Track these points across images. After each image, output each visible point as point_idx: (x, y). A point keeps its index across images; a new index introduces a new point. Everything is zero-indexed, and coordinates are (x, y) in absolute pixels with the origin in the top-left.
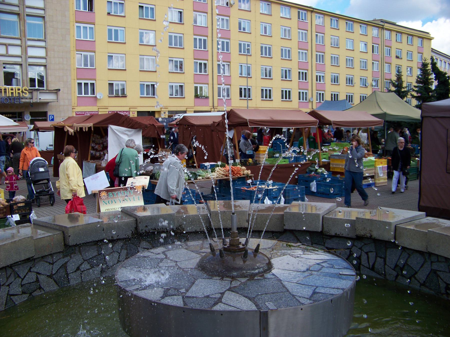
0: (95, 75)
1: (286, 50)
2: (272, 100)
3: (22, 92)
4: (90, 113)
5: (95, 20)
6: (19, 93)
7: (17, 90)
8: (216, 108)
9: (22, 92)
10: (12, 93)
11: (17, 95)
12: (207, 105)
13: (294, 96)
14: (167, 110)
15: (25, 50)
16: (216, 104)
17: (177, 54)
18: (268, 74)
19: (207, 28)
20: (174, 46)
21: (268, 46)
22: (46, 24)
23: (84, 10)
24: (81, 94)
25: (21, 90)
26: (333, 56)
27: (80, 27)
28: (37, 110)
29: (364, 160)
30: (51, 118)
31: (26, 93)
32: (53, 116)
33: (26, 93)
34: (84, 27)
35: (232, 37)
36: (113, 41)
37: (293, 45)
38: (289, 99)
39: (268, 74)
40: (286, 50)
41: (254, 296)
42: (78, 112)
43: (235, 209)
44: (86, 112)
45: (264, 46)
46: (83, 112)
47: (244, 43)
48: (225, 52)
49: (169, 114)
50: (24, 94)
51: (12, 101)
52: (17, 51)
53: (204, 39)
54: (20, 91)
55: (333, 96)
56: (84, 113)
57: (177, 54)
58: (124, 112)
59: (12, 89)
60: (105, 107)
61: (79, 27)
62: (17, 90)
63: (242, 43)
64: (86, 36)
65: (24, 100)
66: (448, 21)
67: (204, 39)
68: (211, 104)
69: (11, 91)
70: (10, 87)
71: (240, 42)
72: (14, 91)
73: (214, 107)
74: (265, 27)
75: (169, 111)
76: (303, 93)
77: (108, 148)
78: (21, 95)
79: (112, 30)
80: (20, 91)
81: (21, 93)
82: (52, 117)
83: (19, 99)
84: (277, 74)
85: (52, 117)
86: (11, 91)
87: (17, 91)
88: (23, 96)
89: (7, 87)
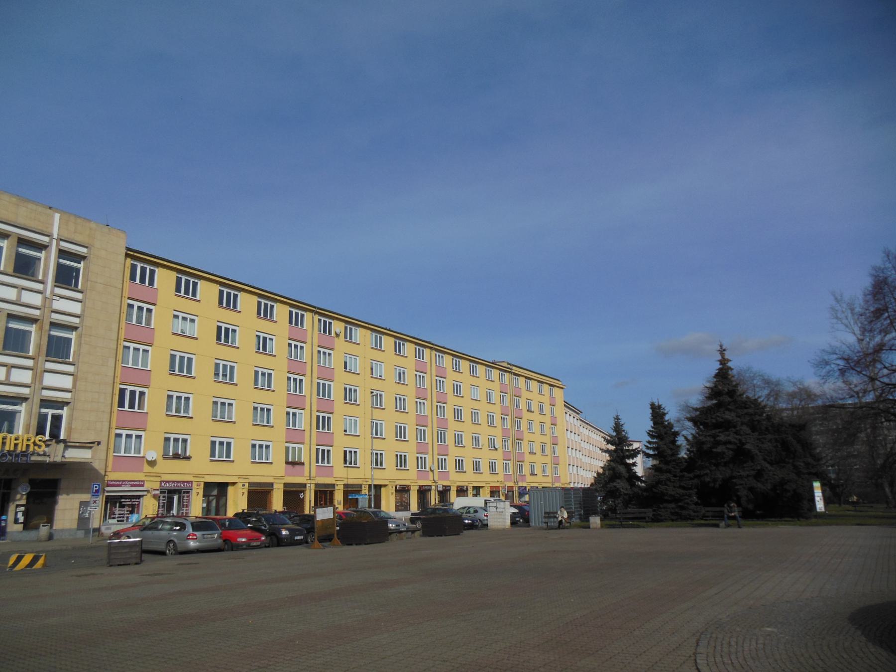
0: (332, 440)
4: (130, 483)
8: (314, 479)
10: (16, 445)
11: (24, 449)
12: (302, 475)
13: (411, 463)
14: (247, 481)
16: (313, 474)
17: (262, 397)
18: (376, 432)
21: (229, 364)
24: (378, 466)
26: (456, 408)
27: (129, 348)
30: (95, 489)
31: (40, 446)
32: (99, 485)
33: (40, 446)
35: (336, 378)
36: (185, 374)
37: (409, 392)
38: (380, 466)
39: (376, 432)
42: (112, 481)
44: (124, 481)
46: (119, 481)
47: (351, 387)
48: (326, 398)
50: (36, 448)
53: (268, 373)
54: (30, 443)
55: (440, 467)
56: (121, 483)
57: (262, 397)
58: (184, 482)
60: (155, 474)
63: (222, 363)
64: (135, 362)
65: (34, 458)
67: (268, 373)
68: (307, 474)
71: (257, 369)
73: (312, 478)
74: (399, 373)
80: (30, 443)
81: (32, 445)
83: (26, 456)
85: (96, 487)
87: (25, 442)
88: (34, 449)
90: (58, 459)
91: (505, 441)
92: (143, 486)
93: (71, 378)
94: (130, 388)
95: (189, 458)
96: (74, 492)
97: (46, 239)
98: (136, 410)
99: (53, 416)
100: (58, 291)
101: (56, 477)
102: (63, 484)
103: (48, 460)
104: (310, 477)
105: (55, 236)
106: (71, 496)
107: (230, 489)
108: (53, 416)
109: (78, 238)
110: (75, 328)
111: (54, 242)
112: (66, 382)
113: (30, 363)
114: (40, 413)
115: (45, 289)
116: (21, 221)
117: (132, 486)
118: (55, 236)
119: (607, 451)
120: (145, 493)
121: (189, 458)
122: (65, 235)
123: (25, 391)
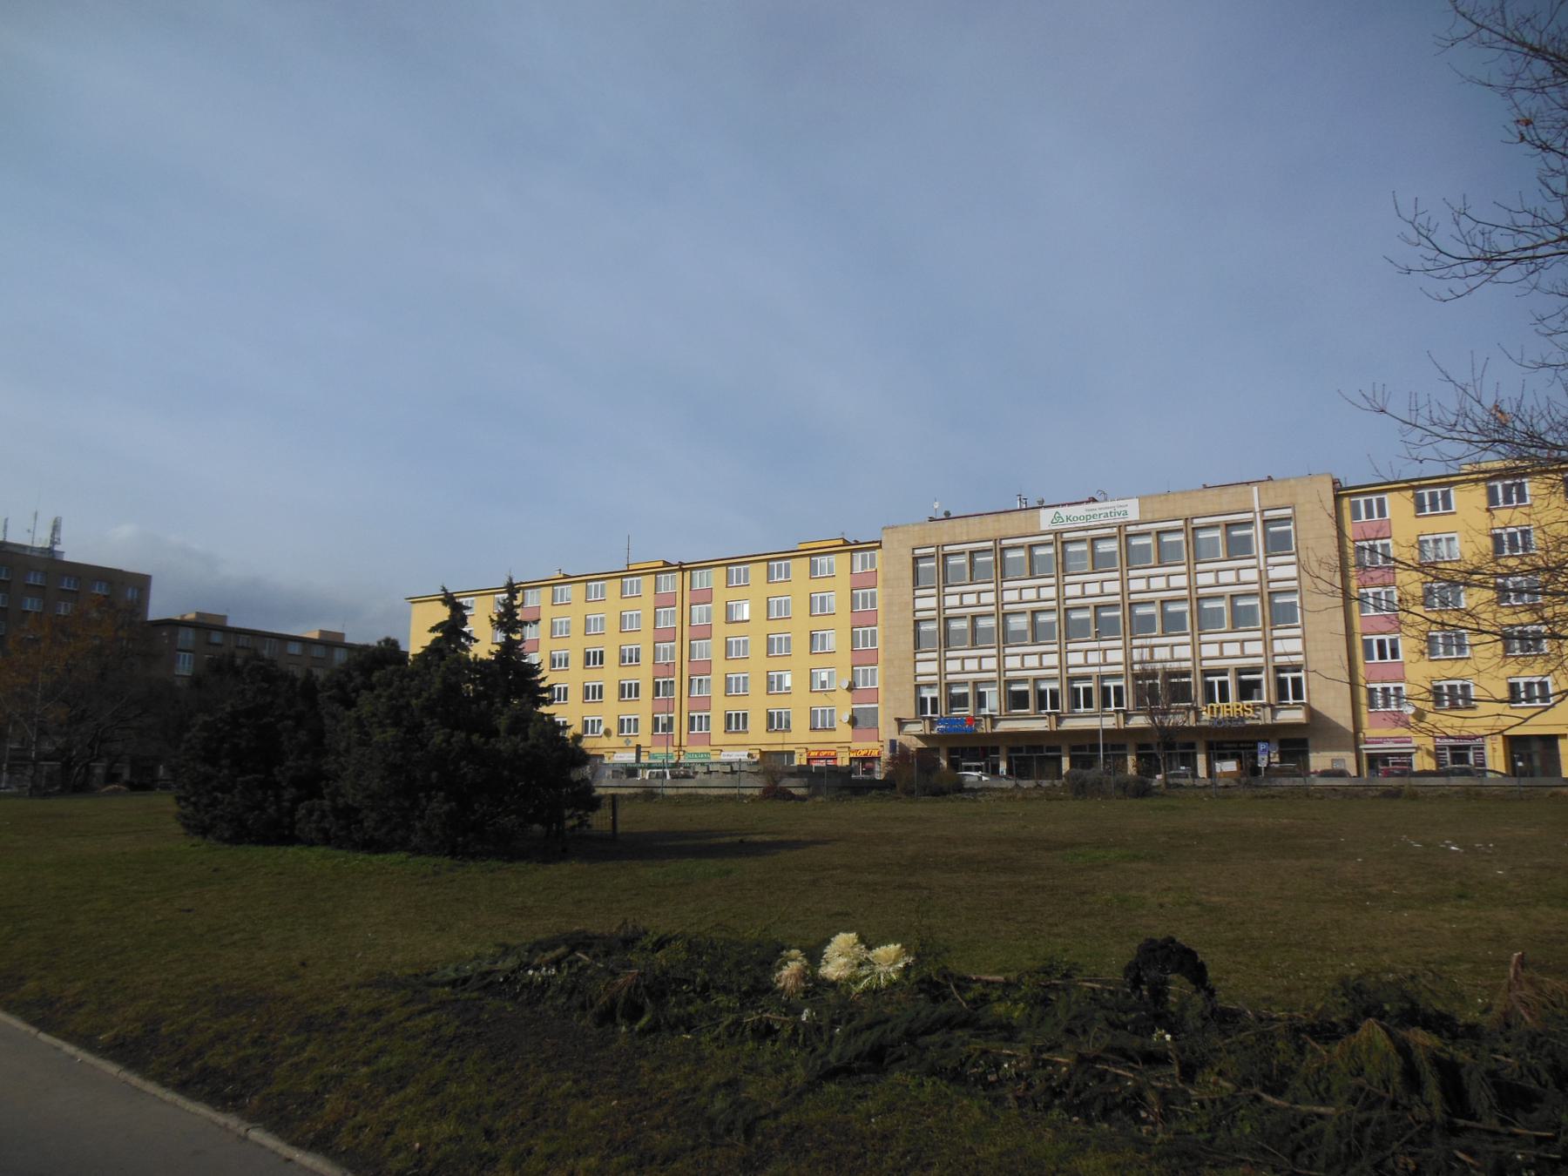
2: (1454, 513)
3: (1244, 710)
9: (1244, 710)
23: (1180, 556)
28: (1290, 736)
29: (453, 740)
31: (1249, 712)
33: (1249, 712)
41: (676, 759)
43: (1230, 1081)
51: (1228, 723)
54: (1240, 709)
59: (1228, 707)
65: (1248, 722)
66: (26, 533)
69: (1236, 709)
70: (1225, 704)
72: (1231, 710)
76: (700, 717)
77: (357, 643)
80: (1240, 709)
84: (594, 677)
86: (1236, 709)
89: (1221, 704)
90: (1269, 721)
91: (630, 661)
92: (1410, 742)
93: (1261, 643)
94: (1375, 638)
95: (834, 730)
96: (1324, 750)
97: (1250, 515)
98: (1389, 659)
99: (1220, 682)
100: (1271, 560)
101: (1305, 736)
102: (1311, 743)
103: (1260, 722)
104: (680, 746)
105: (1257, 509)
106: (1322, 754)
107: (1561, 742)
108: (1220, 682)
109: (1280, 502)
110: (1295, 591)
111: (1258, 514)
112: (1296, 645)
113: (1055, 648)
114: (1010, 692)
115: (1259, 563)
116: (1226, 508)
117: (1396, 742)
118: (1257, 509)
119: (453, 630)
120: (1414, 750)
121: (834, 730)
122: (1266, 504)
123: (1261, 661)
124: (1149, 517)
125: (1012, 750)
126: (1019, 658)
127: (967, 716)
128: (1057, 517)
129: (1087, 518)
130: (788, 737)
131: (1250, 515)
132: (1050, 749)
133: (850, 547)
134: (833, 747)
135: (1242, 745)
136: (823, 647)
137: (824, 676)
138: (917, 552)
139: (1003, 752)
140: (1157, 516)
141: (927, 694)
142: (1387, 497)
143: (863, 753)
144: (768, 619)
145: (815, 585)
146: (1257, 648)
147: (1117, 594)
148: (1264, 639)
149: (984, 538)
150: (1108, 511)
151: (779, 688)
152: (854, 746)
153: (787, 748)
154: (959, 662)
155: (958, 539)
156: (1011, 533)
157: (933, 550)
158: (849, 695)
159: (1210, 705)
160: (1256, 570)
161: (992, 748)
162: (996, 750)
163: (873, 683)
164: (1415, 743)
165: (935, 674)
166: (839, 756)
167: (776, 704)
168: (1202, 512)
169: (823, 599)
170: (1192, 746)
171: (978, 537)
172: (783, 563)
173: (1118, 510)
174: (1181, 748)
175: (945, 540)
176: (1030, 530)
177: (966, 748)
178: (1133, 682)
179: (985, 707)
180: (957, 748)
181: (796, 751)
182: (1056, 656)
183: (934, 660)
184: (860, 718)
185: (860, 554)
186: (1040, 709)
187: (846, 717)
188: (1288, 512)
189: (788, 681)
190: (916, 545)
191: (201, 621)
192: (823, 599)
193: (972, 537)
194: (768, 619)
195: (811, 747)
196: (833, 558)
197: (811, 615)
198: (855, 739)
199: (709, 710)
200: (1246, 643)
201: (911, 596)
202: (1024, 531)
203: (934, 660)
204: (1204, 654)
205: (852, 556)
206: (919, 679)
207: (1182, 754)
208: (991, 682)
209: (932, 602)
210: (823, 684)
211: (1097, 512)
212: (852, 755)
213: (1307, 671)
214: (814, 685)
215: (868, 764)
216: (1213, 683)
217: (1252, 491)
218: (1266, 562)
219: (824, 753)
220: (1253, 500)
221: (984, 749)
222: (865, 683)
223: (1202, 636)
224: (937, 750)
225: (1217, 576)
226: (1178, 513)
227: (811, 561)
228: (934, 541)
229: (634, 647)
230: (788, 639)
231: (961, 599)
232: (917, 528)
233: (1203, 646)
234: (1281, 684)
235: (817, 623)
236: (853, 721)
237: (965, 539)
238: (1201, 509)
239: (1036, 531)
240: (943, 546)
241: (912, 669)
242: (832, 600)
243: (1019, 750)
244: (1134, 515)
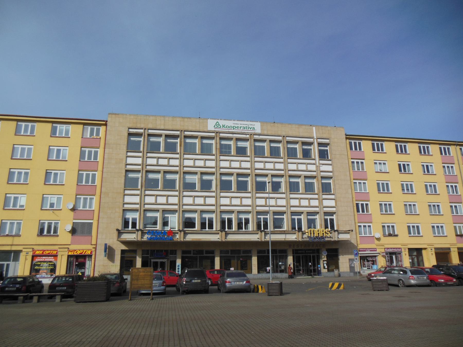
1: (383, 184)
3: (325, 232)
4: (370, 249)
5: (79, 164)
6: (323, 234)
7: (322, 231)
9: (326, 233)
10: (318, 234)
14: (433, 247)
15: (321, 202)
19: (456, 176)
20: (364, 191)
21: (385, 182)
22: (141, 176)
25: (324, 231)
30: (355, 253)
32: (357, 251)
33: (328, 234)
34: (363, 183)
40: (383, 184)
45: (381, 182)
46: (364, 249)
49: (435, 250)
50: (327, 234)
52: (187, 200)
55: (375, 249)
56: (365, 250)
60: (378, 245)
61: (356, 183)
62: (322, 231)
63: (405, 183)
65: (327, 239)
72: (319, 232)
75: (435, 248)
78: (325, 235)
79: (384, 183)
80: (324, 232)
81: (325, 233)
82: (356, 252)
87: (322, 232)
90: (182, 240)
92: (376, 251)
94: (360, 202)
95: (397, 236)
98: (365, 213)
99: (298, 219)
102: (340, 251)
103: (332, 239)
105: (315, 138)
106: (345, 256)
107: (424, 252)
108: (298, 219)
112: (332, 203)
113: (213, 194)
115: (316, 162)
116: (301, 135)
117: (371, 251)
118: (315, 138)
122: (319, 136)
124: (265, 132)
125: (184, 252)
126: (192, 198)
127: (157, 230)
128: (217, 125)
129: (234, 128)
130: (17, 240)
131: (312, 140)
132: (207, 252)
133: (85, 123)
134: (56, 248)
135: (307, 252)
136: (55, 180)
137: (54, 200)
138: (130, 130)
139: (179, 254)
140: (269, 133)
141: (130, 216)
142: (430, 146)
143: (79, 252)
144: (12, 159)
145: (54, 141)
146: (175, 200)
147: (140, 165)
148: (179, 196)
149: (174, 128)
150: (245, 126)
151: (15, 205)
152: (72, 247)
153: (14, 248)
154: (154, 198)
155: (158, 127)
156: (190, 128)
157: (142, 131)
158: (72, 213)
159: (309, 229)
160: (314, 166)
161: (171, 251)
162: (174, 252)
163: (90, 207)
164: (378, 251)
165: (138, 204)
166: (59, 254)
167: (413, 220)
168: (291, 134)
169: (59, 151)
170: (250, 252)
171: (170, 128)
172: (30, 124)
173: (251, 126)
174: (243, 253)
175: (150, 126)
176: (201, 129)
177: (154, 251)
178: (256, 217)
179: (168, 226)
180: (148, 251)
181: (24, 250)
182: (139, 197)
183: (138, 195)
184: (79, 229)
185: (89, 128)
186: (125, 228)
187: (69, 228)
188: (327, 141)
189: (23, 201)
190: (131, 126)
191: (140, 137)
192: (59, 151)
193: (167, 127)
194: (12, 159)
195: (36, 248)
196: (70, 127)
197: (48, 160)
198: (73, 243)
199: (371, 223)
200: (169, 197)
201: (125, 156)
202: (198, 129)
203: (138, 195)
204: (222, 203)
205: (83, 128)
206: (126, 206)
207: (280, 256)
208: (173, 212)
209: (139, 161)
210: (52, 205)
211: (240, 126)
212: (70, 253)
213: (337, 216)
214: (44, 205)
215: (81, 260)
216: (295, 219)
217: (313, 129)
218: (319, 163)
219: (47, 252)
220: (313, 133)
221: (166, 251)
222: (84, 206)
223: (221, 193)
224: (135, 251)
225: (169, 162)
226: (279, 133)
227: (17, 124)
228: (142, 126)
229: (91, 173)
230: (26, 174)
231: (158, 161)
232: (132, 117)
233: (146, 197)
234: (223, 222)
235: (51, 165)
236: (73, 231)
237: (162, 127)
238: (290, 133)
239: (205, 130)
240: (148, 129)
241: (122, 199)
242: (66, 153)
243: (189, 252)
244: (258, 130)
